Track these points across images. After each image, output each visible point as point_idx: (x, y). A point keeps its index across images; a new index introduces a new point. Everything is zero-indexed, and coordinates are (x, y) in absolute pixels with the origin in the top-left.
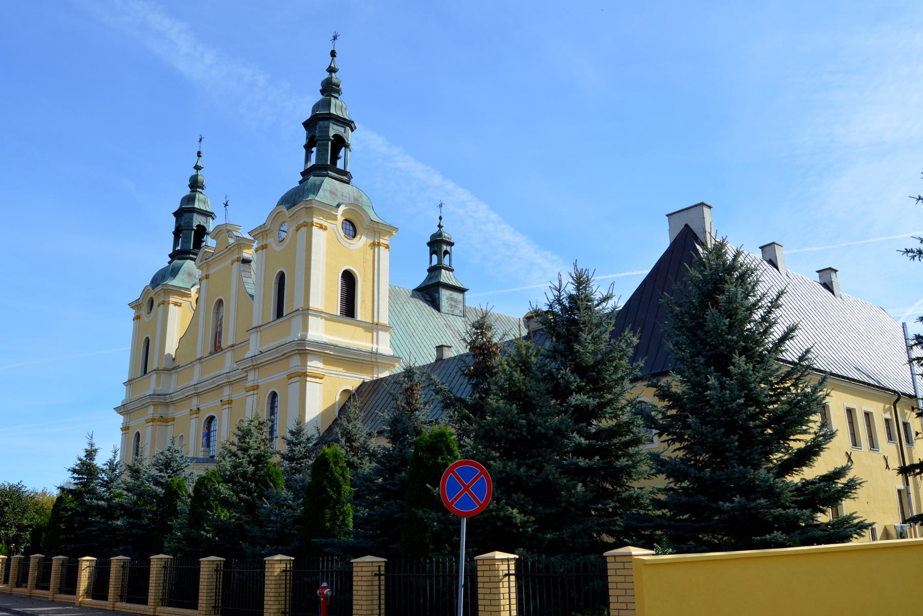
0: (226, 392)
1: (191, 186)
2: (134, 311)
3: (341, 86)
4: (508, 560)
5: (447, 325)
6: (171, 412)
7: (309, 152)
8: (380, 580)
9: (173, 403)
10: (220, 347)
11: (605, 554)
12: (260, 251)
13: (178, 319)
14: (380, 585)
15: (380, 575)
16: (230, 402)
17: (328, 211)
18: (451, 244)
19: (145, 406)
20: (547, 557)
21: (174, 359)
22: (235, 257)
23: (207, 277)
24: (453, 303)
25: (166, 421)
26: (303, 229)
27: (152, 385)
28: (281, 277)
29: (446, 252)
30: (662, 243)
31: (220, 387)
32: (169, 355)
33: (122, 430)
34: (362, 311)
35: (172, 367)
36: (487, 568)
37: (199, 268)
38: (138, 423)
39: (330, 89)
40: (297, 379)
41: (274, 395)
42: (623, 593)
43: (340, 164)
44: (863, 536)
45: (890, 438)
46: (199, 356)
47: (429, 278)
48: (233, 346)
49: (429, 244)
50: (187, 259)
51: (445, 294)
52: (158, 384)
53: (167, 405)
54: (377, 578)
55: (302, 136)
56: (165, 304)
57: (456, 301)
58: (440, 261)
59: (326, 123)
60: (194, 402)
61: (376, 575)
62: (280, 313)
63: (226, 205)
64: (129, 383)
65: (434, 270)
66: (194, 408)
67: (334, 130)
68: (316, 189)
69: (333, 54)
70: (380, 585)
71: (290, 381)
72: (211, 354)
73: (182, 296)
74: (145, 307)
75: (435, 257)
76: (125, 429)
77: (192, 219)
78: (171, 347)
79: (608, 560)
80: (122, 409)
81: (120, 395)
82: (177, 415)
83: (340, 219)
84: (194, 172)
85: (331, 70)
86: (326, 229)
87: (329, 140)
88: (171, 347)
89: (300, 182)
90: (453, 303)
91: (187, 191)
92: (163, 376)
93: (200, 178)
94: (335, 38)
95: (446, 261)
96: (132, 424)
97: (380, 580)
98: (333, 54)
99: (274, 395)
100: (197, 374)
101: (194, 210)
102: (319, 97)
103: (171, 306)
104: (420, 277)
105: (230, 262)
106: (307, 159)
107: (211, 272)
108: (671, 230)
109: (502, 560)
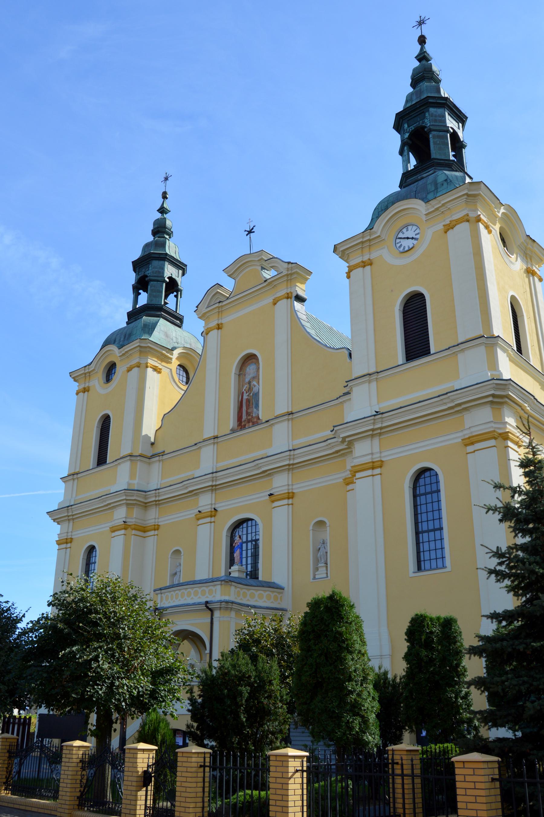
0: (280, 483)
1: (155, 233)
4: (205, 753)
6: (152, 516)
7: (137, 295)
8: (204, 772)
9: (157, 503)
11: (177, 751)
12: (81, 394)
13: (159, 393)
14: (204, 777)
15: (204, 766)
16: (290, 496)
17: (162, 353)
19: (111, 507)
21: (153, 444)
22: (283, 293)
23: (219, 327)
25: (144, 529)
26: (136, 370)
27: (120, 477)
28: (106, 422)
31: (268, 474)
32: (147, 437)
33: (59, 543)
35: (151, 454)
36: (280, 764)
38: (87, 533)
39: (160, 230)
40: (492, 442)
41: (91, 549)
42: (473, 799)
46: (209, 433)
48: (216, 437)
52: (132, 475)
53: (146, 506)
54: (202, 769)
55: (132, 277)
56: (142, 367)
59: (440, 111)
60: (205, 502)
61: (201, 766)
62: (102, 459)
64: (72, 477)
66: (206, 509)
67: (170, 271)
68: (150, 329)
69: (164, 196)
70: (204, 777)
71: (470, 449)
72: (233, 431)
73: (162, 361)
74: (100, 375)
76: (64, 542)
77: (163, 269)
78: (150, 425)
79: (179, 755)
80: (62, 515)
81: (57, 495)
82: (163, 521)
83: (175, 363)
84: (159, 216)
85: (162, 210)
86: (159, 372)
87: (165, 281)
88: (150, 425)
92: (140, 465)
93: (168, 223)
96: (78, 534)
97: (204, 772)
99: (91, 549)
100: (207, 460)
101: (165, 258)
102: (150, 238)
103: (149, 370)
105: (270, 300)
106: (136, 301)
107: (226, 320)
109: (143, 750)
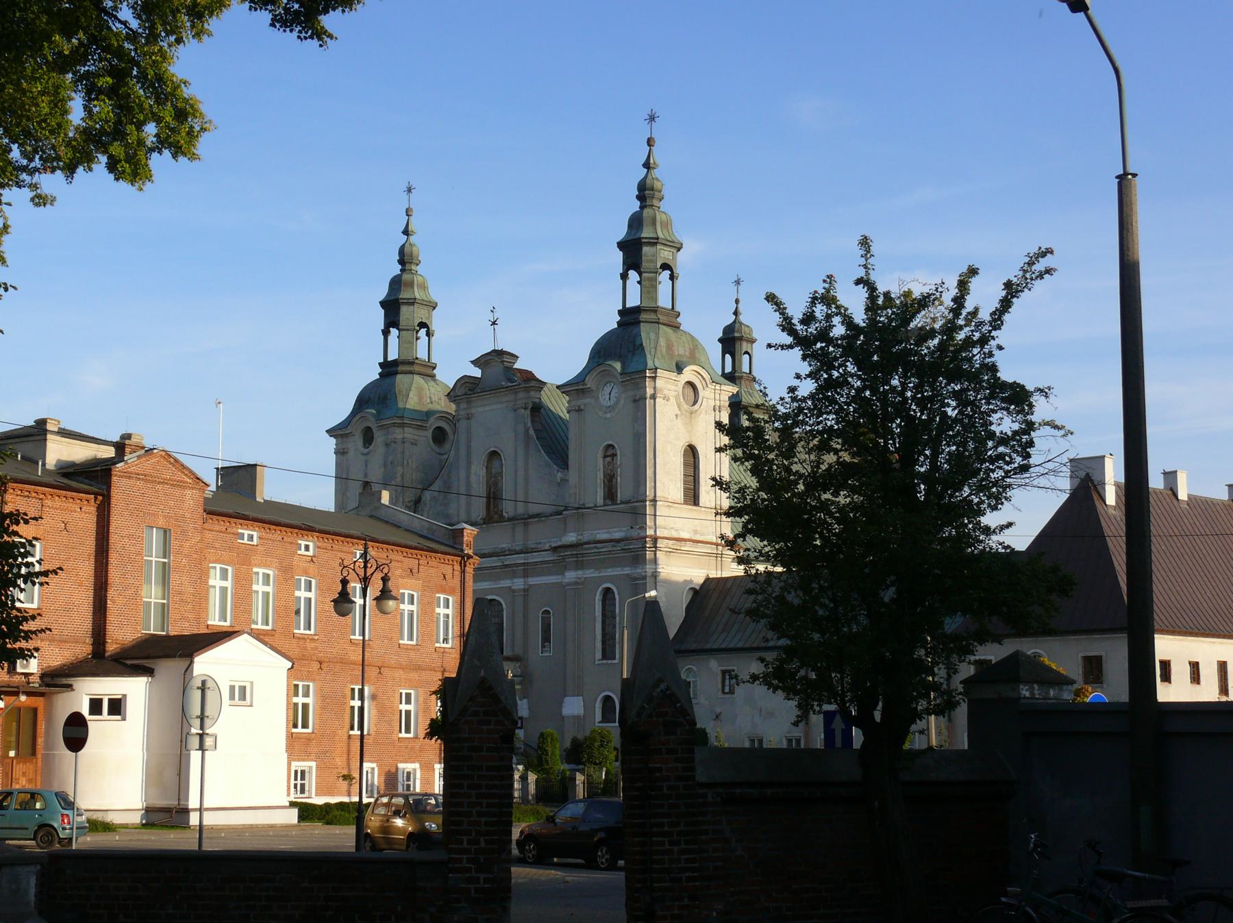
2: (333, 441)
74: (358, 441)
91: (396, 269)
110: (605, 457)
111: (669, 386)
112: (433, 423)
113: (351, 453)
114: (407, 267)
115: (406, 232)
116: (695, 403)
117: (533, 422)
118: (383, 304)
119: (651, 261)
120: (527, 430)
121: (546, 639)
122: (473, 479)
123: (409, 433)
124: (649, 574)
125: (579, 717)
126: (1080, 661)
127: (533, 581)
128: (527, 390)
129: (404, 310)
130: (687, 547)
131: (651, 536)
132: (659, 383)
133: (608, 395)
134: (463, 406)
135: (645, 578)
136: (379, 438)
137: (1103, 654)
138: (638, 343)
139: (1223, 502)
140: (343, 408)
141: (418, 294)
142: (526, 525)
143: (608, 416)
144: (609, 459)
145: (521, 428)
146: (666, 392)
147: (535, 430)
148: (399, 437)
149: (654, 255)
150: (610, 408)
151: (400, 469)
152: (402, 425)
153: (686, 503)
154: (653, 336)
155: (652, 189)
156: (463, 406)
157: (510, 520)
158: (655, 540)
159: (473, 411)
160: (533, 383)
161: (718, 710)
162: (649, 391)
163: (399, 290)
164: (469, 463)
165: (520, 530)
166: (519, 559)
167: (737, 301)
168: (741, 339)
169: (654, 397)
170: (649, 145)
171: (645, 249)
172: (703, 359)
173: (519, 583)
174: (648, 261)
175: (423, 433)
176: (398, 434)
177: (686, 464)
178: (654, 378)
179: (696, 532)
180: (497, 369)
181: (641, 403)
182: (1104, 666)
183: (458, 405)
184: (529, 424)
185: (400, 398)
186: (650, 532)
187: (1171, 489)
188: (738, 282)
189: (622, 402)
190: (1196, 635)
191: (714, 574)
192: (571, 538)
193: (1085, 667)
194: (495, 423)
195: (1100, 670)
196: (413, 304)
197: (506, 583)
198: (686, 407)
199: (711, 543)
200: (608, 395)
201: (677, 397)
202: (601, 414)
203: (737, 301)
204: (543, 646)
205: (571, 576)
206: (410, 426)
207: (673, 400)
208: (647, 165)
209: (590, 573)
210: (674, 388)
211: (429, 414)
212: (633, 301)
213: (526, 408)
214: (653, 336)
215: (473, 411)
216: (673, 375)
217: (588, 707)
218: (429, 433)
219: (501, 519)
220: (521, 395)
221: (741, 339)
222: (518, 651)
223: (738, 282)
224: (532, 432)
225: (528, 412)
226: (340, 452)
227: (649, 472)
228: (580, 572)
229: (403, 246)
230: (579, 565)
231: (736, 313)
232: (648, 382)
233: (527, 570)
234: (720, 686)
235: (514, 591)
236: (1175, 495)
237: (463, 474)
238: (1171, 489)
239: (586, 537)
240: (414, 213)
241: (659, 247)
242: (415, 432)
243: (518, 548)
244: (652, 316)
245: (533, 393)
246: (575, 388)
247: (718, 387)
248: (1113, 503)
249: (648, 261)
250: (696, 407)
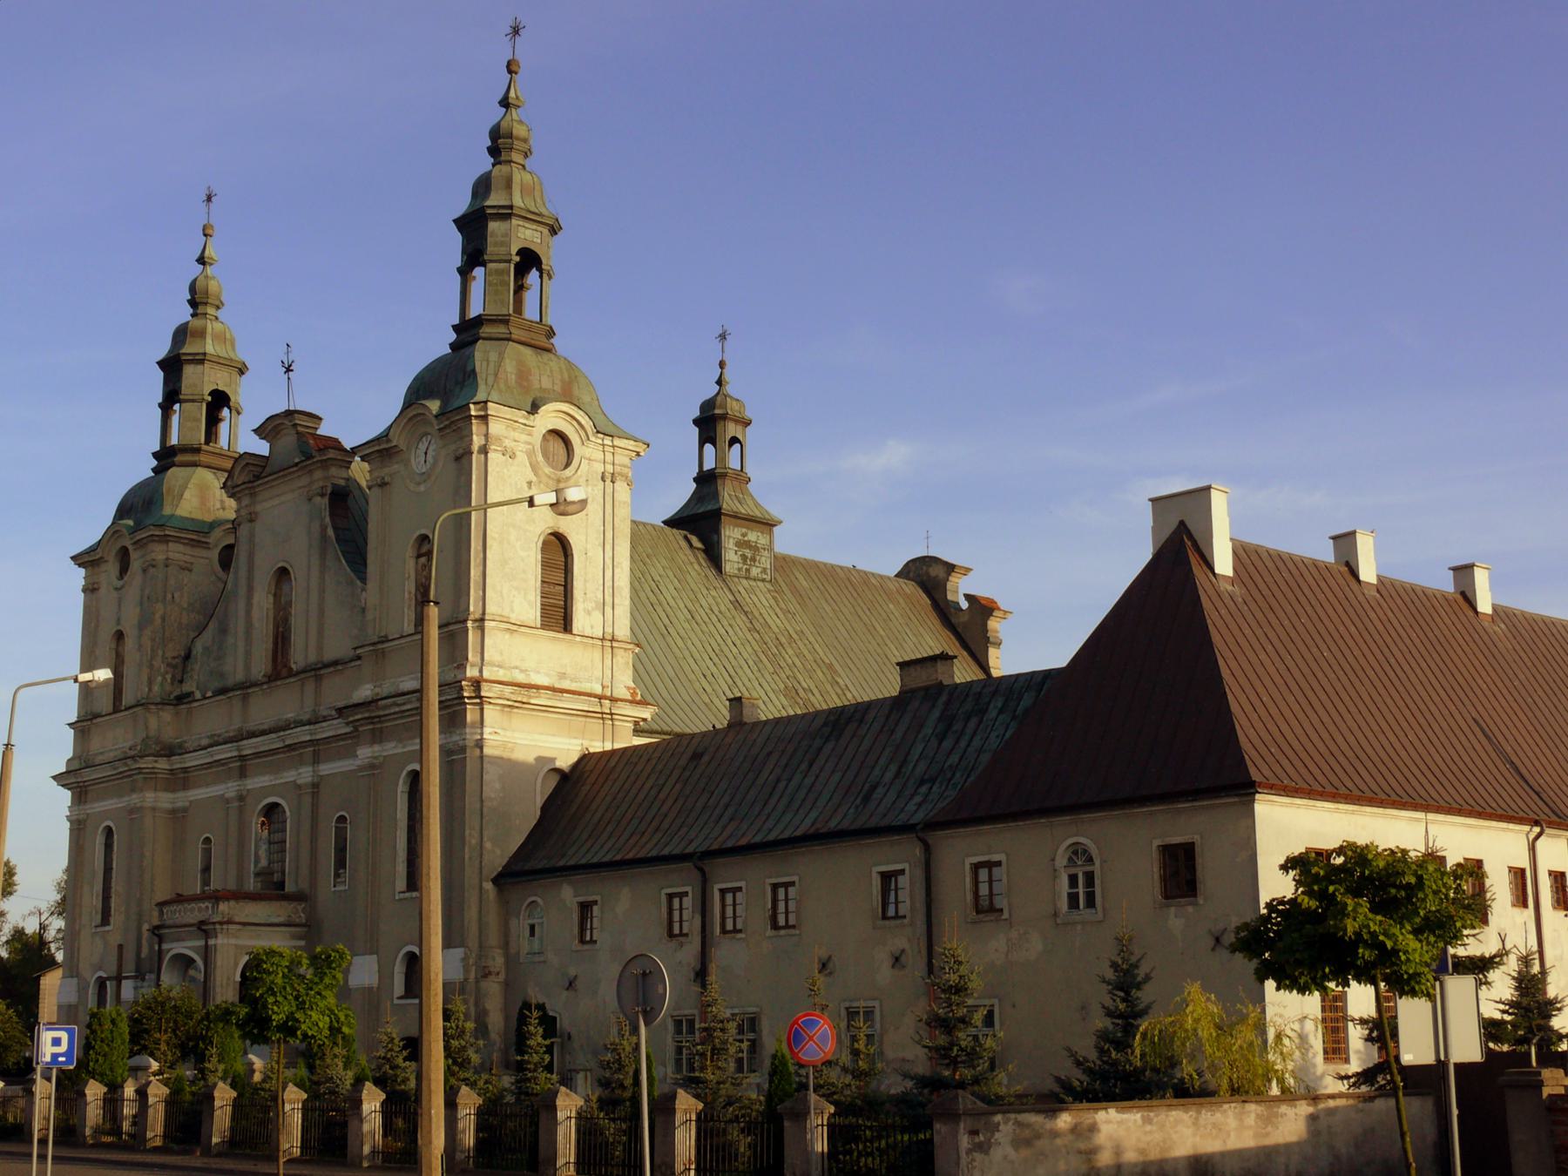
2: (82, 571)
3: (531, 142)
5: (737, 604)
10: (286, 665)
18: (747, 423)
20: (931, 1093)
24: (748, 553)
29: (734, 440)
30: (1142, 554)
34: (584, 619)
37: (231, 496)
43: (530, 311)
44: (1058, 1080)
45: (1521, 900)
47: (697, 497)
49: (696, 422)
50: (195, 465)
51: (730, 535)
57: (755, 548)
58: (721, 458)
63: (288, 370)
65: (707, 481)
69: (511, 68)
74: (112, 568)
75: (708, 448)
89: (453, 346)
90: (748, 553)
91: (184, 314)
94: (516, 31)
95: (733, 461)
98: (511, 68)
104: (678, 493)
108: (1156, 530)
110: (419, 556)
111: (516, 435)
112: (219, 539)
113: (103, 591)
114: (201, 309)
115: (201, 260)
116: (568, 465)
117: (332, 515)
118: (163, 364)
119: (502, 244)
120: (324, 529)
121: (341, 863)
122: (256, 613)
123: (177, 552)
124: (470, 743)
125: (370, 989)
126: (1155, 855)
127: (326, 769)
128: (325, 464)
129: (189, 371)
130: (543, 699)
131: (470, 680)
132: (495, 427)
133: (423, 456)
134: (246, 501)
135: (463, 749)
136: (136, 565)
137: (1197, 838)
138: (469, 368)
139: (1444, 596)
140: (94, 525)
141: (210, 348)
142: (318, 678)
143: (422, 488)
144: (423, 560)
145: (316, 527)
146: (507, 443)
147: (335, 528)
148: (161, 557)
149: (507, 235)
150: (426, 476)
151: (159, 606)
152: (165, 539)
153: (544, 626)
154: (493, 357)
155: (510, 136)
156: (246, 501)
157: (298, 673)
158: (477, 684)
159: (258, 508)
160: (332, 454)
161: (572, 972)
162: (477, 441)
163: (183, 343)
164: (250, 589)
165: (310, 687)
166: (302, 734)
167: (722, 365)
168: (724, 417)
169: (484, 451)
170: (510, 72)
171: (493, 226)
172: (586, 398)
173: (305, 775)
174: (496, 244)
175: (204, 553)
176: (159, 552)
177: (546, 565)
178: (484, 418)
179: (562, 676)
180: (288, 440)
181: (464, 461)
182: (1199, 860)
183: (238, 500)
184: (328, 519)
185: (167, 501)
186: (471, 672)
187: (1347, 564)
188: (723, 337)
189: (441, 464)
190: (1381, 804)
191: (597, 747)
192: (365, 692)
193: (1164, 866)
194: (289, 524)
195: (1192, 868)
196: (201, 362)
197: (289, 776)
198: (548, 470)
199: (595, 696)
200: (423, 456)
201: (530, 454)
202: (412, 487)
203: (722, 365)
204: (337, 875)
205: (365, 753)
206: (178, 540)
207: (522, 457)
208: (505, 103)
209: (390, 748)
210: (524, 437)
211: (213, 525)
212: (709, 464)
213: (322, 495)
214: (493, 357)
215: (258, 508)
216: (520, 416)
217: (385, 974)
218: (215, 554)
219: (291, 674)
220: (318, 474)
221: (724, 417)
222: (304, 885)
223: (723, 337)
224: (330, 532)
225: (326, 500)
226: (90, 589)
227: (475, 573)
228: (377, 748)
229: (194, 281)
230: (377, 737)
231: (719, 382)
232: (476, 426)
233: (318, 751)
234: (576, 930)
235: (299, 787)
236: (1354, 573)
237: (242, 605)
238: (1347, 564)
239: (386, 689)
240: (216, 233)
241: (515, 221)
242: (188, 550)
243: (305, 717)
244: (500, 330)
245: (333, 471)
246: (380, 450)
247: (608, 441)
248: (1229, 572)
249: (496, 244)
250: (569, 472)
